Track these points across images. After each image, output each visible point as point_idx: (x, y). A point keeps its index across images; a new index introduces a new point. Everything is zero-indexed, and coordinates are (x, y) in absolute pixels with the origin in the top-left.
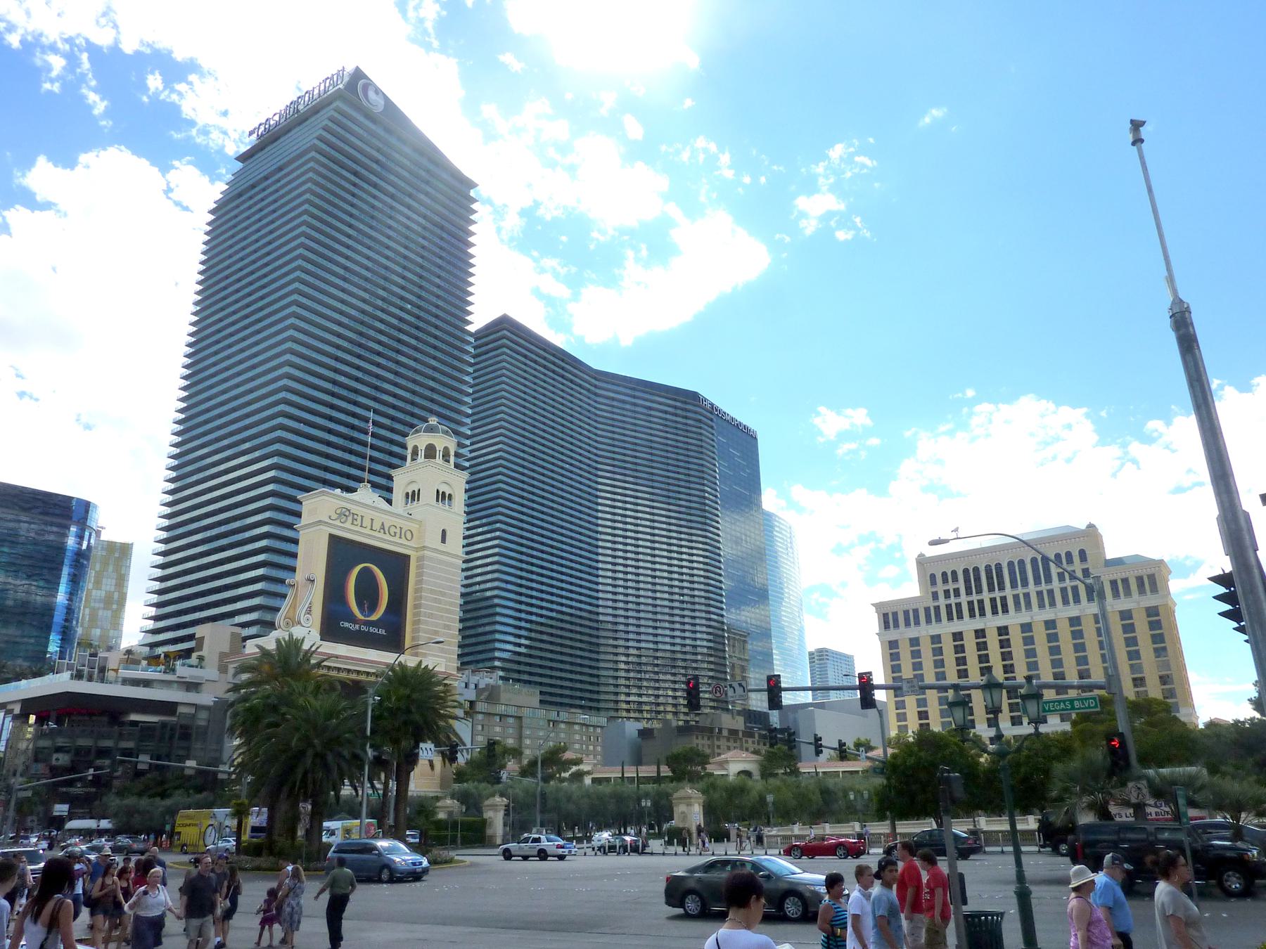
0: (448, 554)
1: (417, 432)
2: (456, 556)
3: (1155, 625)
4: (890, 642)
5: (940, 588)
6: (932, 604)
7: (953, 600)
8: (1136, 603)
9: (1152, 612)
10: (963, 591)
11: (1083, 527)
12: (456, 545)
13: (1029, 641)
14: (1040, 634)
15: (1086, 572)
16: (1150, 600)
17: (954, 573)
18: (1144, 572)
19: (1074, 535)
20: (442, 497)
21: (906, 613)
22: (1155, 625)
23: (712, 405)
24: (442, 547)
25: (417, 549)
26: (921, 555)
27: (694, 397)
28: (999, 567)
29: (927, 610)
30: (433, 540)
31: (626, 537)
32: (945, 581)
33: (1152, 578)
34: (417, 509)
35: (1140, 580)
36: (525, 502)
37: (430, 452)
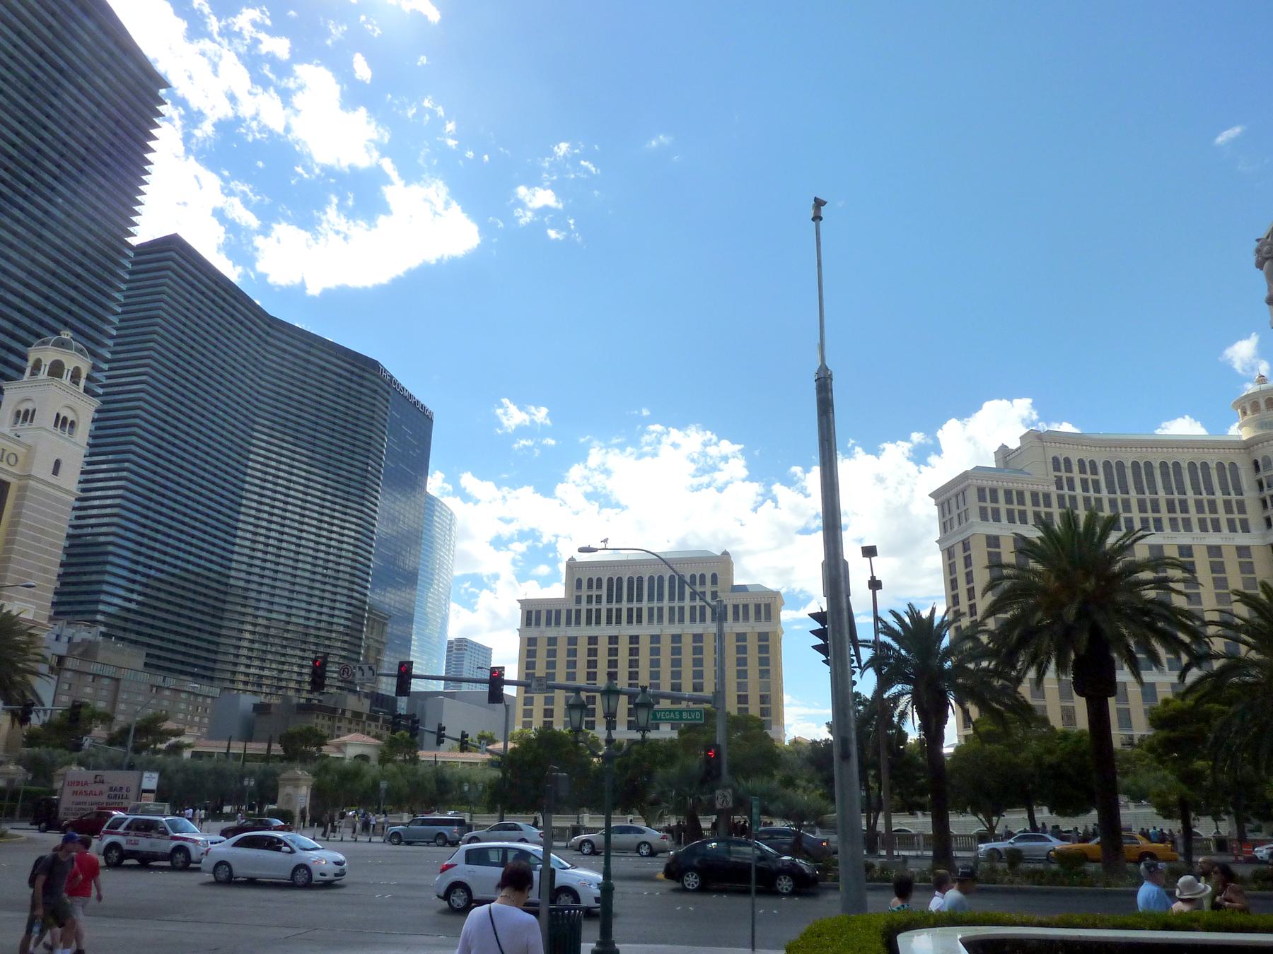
0: (59, 488)
1: (44, 343)
2: (68, 492)
3: (764, 649)
4: (529, 639)
5: (584, 593)
6: (574, 607)
7: (594, 606)
8: (750, 627)
9: (763, 637)
10: (604, 598)
12: (70, 480)
13: (614, 652)
14: (623, 648)
15: (714, 595)
16: (763, 627)
17: (599, 580)
18: (763, 601)
19: (705, 559)
20: (62, 423)
21: (549, 612)
22: (764, 649)
23: (392, 377)
24: (52, 479)
25: (20, 477)
27: (374, 365)
28: (640, 579)
29: (569, 612)
30: (42, 469)
31: (275, 492)
32: (590, 586)
33: (768, 606)
34: (28, 433)
35: (758, 607)
36: (164, 444)
37: (56, 369)
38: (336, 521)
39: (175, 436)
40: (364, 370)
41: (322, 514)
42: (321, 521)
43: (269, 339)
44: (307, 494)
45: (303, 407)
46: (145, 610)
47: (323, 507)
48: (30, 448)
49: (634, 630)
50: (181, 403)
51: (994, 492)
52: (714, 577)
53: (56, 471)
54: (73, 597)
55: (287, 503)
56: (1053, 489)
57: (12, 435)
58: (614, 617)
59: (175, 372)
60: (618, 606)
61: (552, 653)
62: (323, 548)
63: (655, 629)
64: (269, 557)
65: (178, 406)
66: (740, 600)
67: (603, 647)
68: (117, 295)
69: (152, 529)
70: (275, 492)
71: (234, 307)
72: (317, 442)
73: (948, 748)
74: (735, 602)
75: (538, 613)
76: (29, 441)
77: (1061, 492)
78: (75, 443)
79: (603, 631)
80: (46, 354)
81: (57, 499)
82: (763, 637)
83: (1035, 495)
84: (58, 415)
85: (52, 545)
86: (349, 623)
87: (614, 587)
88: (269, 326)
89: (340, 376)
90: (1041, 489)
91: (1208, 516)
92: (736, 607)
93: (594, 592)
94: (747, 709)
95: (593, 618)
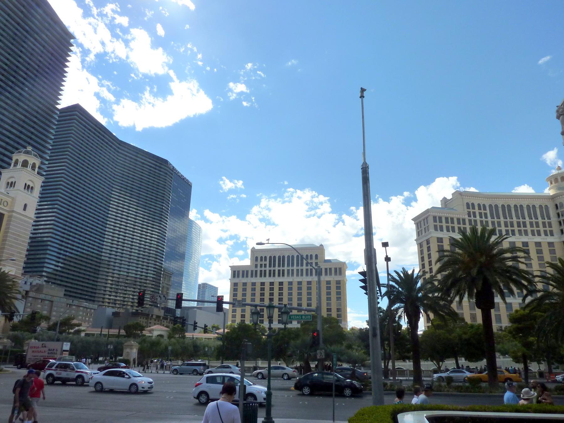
0: (26, 216)
1: (19, 152)
2: (30, 218)
3: (338, 288)
4: (235, 283)
5: (259, 263)
6: (254, 269)
7: (263, 269)
8: (332, 278)
9: (338, 282)
10: (268, 265)
11: (318, 246)
12: (31, 213)
13: (272, 289)
14: (276, 287)
15: (316, 264)
16: (338, 278)
17: (265, 257)
18: (338, 267)
19: (312, 248)
20: (27, 187)
21: (243, 272)
22: (338, 288)
23: (173, 167)
24: (23, 212)
25: (9, 212)
26: (445, 198)
27: (166, 162)
28: (284, 257)
29: (252, 271)
30: (19, 208)
31: (122, 218)
32: (261, 260)
33: (340, 269)
34: (12, 192)
35: (336, 269)
37: (25, 164)
38: (149, 231)
39: (77, 193)
40: (161, 164)
41: (143, 228)
42: (142, 231)
43: (119, 150)
44: (136, 219)
45: (134, 181)
46: (64, 270)
47: (143, 225)
48: (13, 199)
49: (281, 279)
50: (80, 179)
51: (440, 218)
52: (316, 256)
53: (25, 209)
54: (32, 265)
55: (127, 223)
56: (466, 217)
57: (5, 193)
58: (272, 274)
59: (78, 165)
60: (274, 269)
61: (244, 290)
62: (143, 243)
63: (290, 279)
64: (119, 247)
65: (79, 180)
66: (328, 266)
67: (267, 287)
68: (52, 131)
69: (67, 235)
70: (122, 218)
71: (104, 136)
72: (140, 196)
73: (420, 332)
74: (326, 267)
75: (238, 272)
76: (13, 196)
77: (470, 218)
78: (33, 197)
79: (267, 280)
80: (21, 157)
81: (25, 221)
82: (338, 282)
83: (458, 220)
84: (26, 184)
85: (23, 242)
86: (155, 276)
87: (272, 260)
88: (119, 144)
89: (151, 167)
90: (461, 217)
91: (535, 229)
92: (326, 269)
93: (263, 263)
94: (331, 314)
95: (263, 274)
